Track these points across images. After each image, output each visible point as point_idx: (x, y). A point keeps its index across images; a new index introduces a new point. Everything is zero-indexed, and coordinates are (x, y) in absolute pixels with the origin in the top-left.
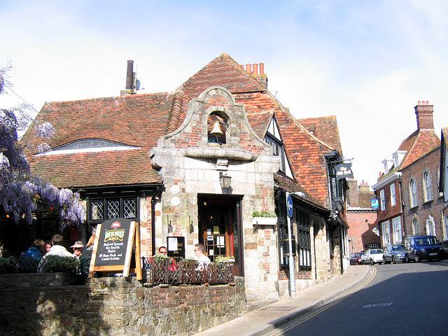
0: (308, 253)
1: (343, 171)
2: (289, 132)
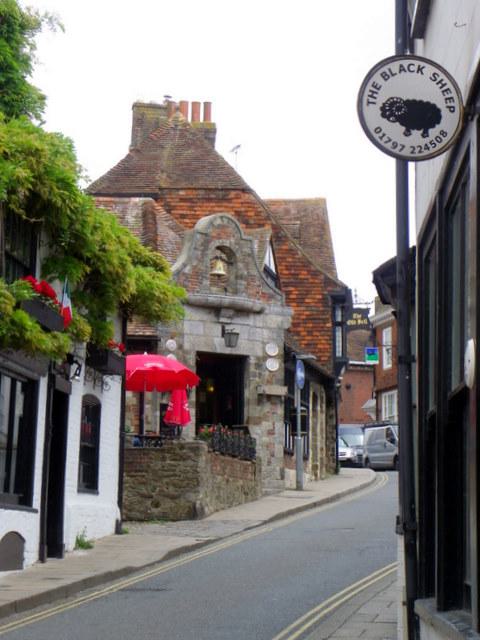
1: (356, 320)
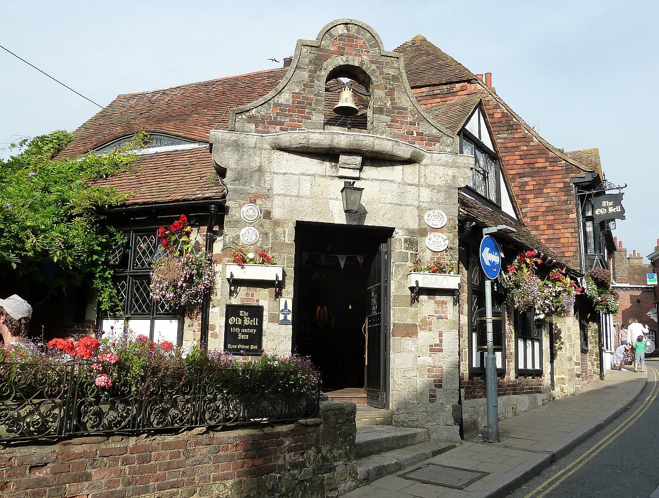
0: (537, 344)
1: (607, 208)
2: (514, 144)
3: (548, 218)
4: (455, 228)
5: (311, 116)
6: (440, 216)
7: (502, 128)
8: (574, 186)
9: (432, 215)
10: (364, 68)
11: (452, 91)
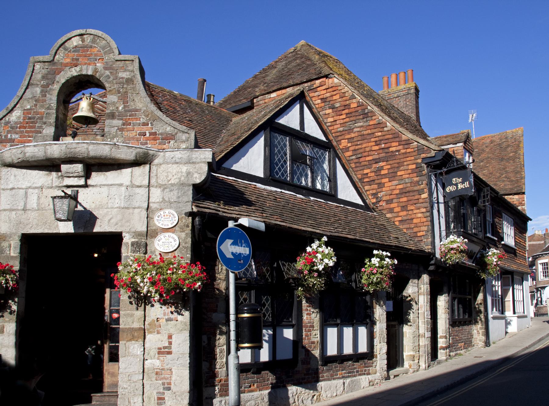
2: (369, 131)
3: (401, 200)
4: (188, 226)
5: (41, 130)
6: (171, 215)
7: (358, 117)
8: (425, 166)
9: (163, 216)
10: (97, 75)
11: (312, 88)
